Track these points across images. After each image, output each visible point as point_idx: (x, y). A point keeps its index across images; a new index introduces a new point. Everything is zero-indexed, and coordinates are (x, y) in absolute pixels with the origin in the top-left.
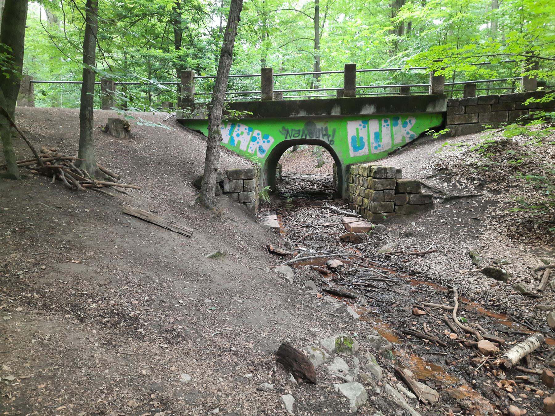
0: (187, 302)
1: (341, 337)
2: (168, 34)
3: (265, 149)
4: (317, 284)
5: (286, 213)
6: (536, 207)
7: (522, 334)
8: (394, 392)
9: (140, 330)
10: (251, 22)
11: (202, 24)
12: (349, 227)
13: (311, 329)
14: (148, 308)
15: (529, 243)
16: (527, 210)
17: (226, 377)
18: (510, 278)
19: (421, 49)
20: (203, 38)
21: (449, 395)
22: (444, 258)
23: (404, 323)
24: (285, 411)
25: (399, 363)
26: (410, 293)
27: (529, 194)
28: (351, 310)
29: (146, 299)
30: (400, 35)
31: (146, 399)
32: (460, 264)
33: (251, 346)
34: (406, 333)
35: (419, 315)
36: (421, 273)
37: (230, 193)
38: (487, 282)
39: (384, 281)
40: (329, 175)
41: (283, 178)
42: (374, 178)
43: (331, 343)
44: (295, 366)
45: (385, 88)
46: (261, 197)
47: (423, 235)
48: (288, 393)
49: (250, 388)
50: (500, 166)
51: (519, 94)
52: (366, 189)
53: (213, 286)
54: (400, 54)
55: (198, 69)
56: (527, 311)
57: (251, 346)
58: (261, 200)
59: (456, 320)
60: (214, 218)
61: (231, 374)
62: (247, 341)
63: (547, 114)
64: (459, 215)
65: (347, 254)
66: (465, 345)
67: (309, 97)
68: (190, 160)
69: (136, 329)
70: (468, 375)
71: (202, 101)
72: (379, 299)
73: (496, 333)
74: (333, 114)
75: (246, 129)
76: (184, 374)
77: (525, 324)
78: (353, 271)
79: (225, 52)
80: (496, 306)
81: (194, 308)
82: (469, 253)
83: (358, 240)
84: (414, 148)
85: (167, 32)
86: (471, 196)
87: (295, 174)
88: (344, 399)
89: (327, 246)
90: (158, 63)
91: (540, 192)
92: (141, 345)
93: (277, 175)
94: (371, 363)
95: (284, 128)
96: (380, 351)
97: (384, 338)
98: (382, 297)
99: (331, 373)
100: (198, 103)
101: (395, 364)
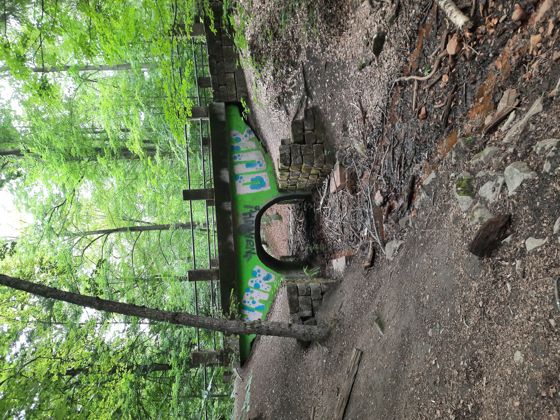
0: (434, 355)
1: (457, 191)
2: (156, 378)
3: (266, 273)
4: (402, 215)
5: (330, 250)
6: (311, 13)
7: (438, 14)
8: (512, 133)
9: (470, 408)
10: (144, 293)
11: (147, 342)
12: (340, 186)
13: (451, 221)
14: (444, 400)
15: (346, 15)
16: (315, 20)
17: (513, 312)
18: (382, 29)
19: (168, 130)
20: (160, 341)
21: (508, 79)
22: (366, 92)
23: (436, 127)
24: (544, 247)
25: (479, 130)
26: (404, 122)
27: (299, 20)
28: (427, 179)
29: (434, 402)
30: (155, 150)
31: (549, 403)
32: (371, 77)
33: (476, 285)
34: (447, 124)
35: (427, 113)
36: (382, 113)
37: (313, 310)
38: (388, 51)
39: (393, 149)
40: (289, 208)
41: (294, 254)
42: (290, 166)
43: (464, 201)
44: (494, 237)
45: (204, 161)
46: (314, 276)
47: (345, 114)
48: (524, 244)
49: (523, 285)
50: (274, 49)
51: (207, 38)
52: (301, 172)
53: (413, 326)
54: (173, 149)
55: (190, 345)
56: (414, 11)
57: (476, 285)
58: (318, 276)
59: (428, 77)
60: (339, 327)
61: (509, 306)
62: (471, 289)
63: (225, 13)
64: (323, 82)
65: (368, 188)
66: (454, 67)
67: (215, 232)
68: (281, 353)
69: (468, 412)
70: (485, 62)
71: (221, 341)
72: (413, 152)
73: (439, 38)
74: (230, 208)
75: (248, 295)
76: (515, 359)
77: (427, 12)
78: (386, 180)
79: (174, 319)
80: (411, 40)
81: (440, 347)
82: (360, 70)
83: (353, 177)
84: (259, 129)
85: (154, 379)
86: (304, 72)
87: (289, 242)
88: (524, 185)
89: (361, 207)
90: (185, 388)
91: (296, 11)
92: (486, 407)
93: (291, 260)
94: (482, 158)
95: (246, 256)
96: (468, 149)
97: (454, 146)
98: (411, 150)
99: (497, 200)
100: (224, 345)
101: (481, 134)
